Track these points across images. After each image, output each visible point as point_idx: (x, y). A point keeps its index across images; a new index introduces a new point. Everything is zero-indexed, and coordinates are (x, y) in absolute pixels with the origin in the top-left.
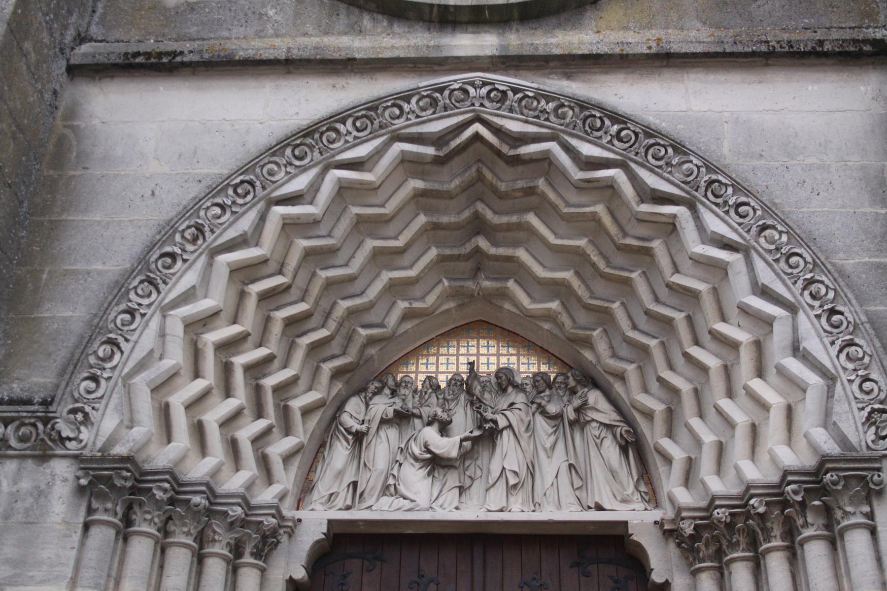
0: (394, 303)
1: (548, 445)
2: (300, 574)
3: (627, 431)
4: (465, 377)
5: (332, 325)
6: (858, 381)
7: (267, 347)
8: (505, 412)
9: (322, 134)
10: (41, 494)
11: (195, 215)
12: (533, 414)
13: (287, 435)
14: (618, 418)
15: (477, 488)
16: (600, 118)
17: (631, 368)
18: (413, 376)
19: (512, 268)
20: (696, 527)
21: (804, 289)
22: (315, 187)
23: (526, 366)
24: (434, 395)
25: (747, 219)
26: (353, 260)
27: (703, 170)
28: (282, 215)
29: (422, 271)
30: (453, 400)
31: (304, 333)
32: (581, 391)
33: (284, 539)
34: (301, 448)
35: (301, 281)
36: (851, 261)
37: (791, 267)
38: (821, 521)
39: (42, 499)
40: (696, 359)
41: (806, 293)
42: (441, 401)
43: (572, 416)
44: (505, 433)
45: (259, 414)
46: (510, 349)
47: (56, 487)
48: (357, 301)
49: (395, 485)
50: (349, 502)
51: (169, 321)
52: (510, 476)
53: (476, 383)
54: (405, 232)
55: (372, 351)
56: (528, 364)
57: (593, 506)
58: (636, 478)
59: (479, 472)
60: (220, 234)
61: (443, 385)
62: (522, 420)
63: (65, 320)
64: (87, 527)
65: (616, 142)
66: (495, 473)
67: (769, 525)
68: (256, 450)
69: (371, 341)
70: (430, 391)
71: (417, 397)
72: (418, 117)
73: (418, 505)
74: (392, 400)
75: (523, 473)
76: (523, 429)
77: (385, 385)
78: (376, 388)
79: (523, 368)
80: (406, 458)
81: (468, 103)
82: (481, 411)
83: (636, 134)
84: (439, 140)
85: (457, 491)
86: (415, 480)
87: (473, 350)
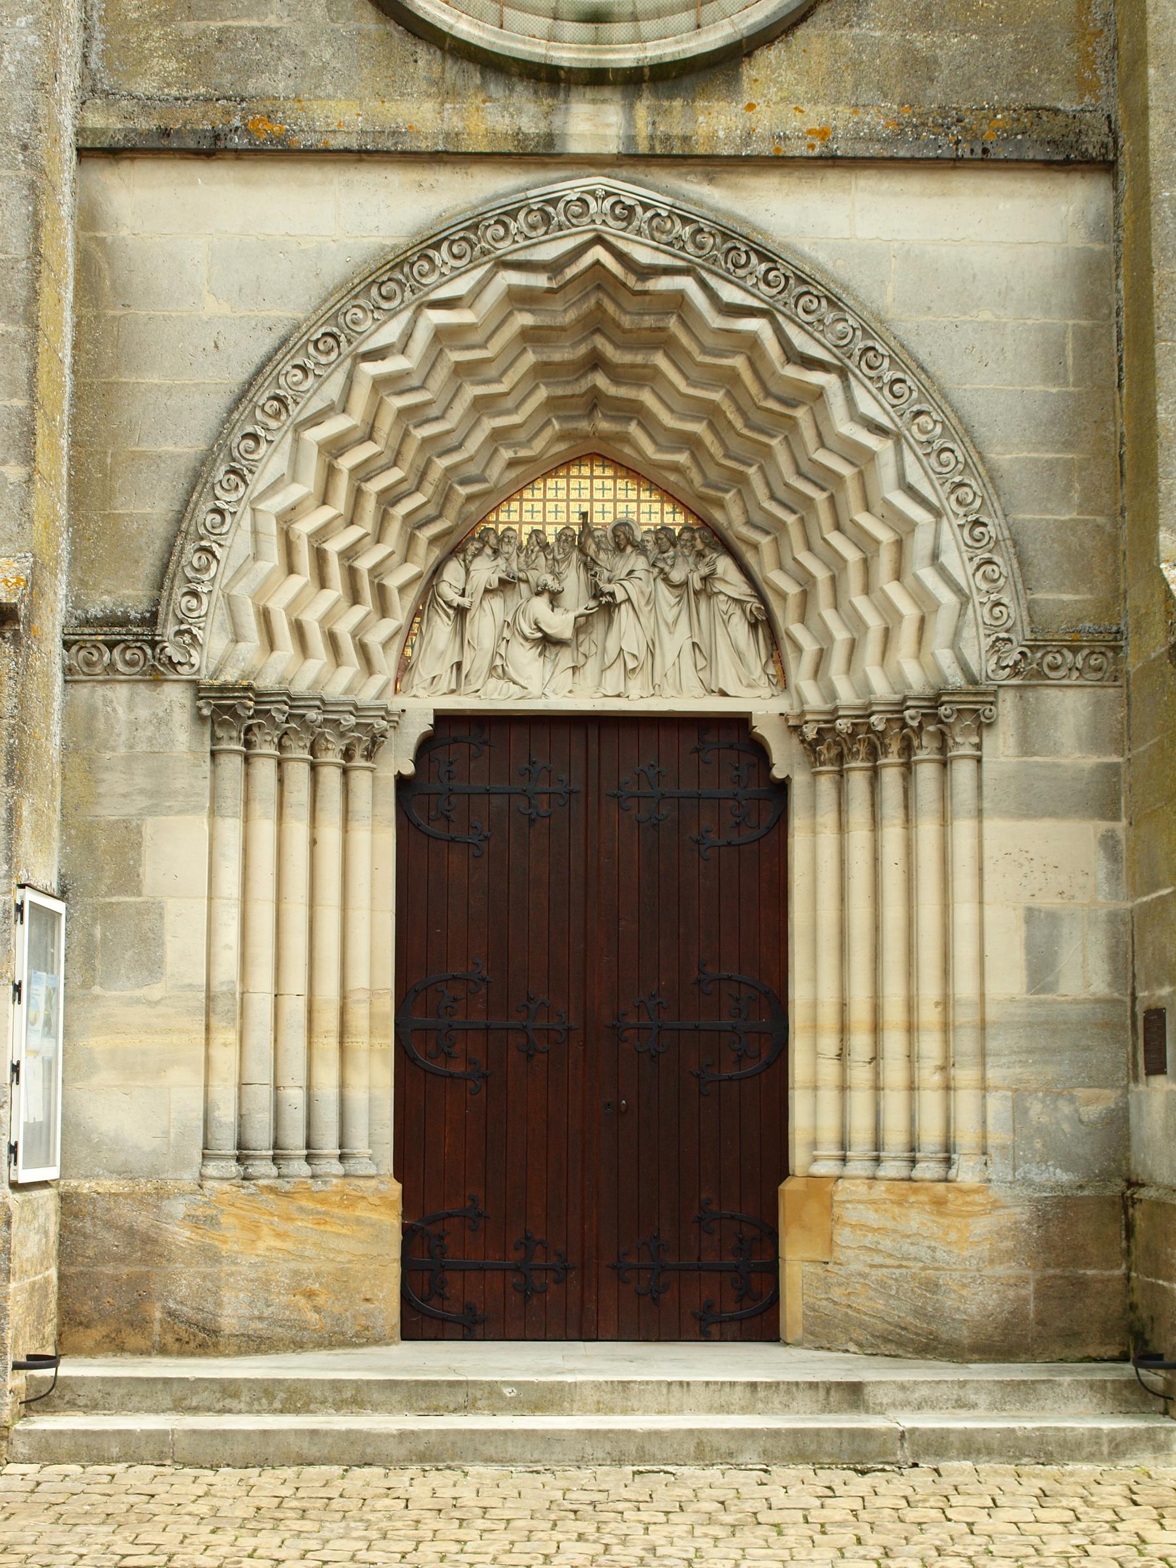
0: (496, 450)
1: (670, 620)
2: (409, 769)
3: (759, 609)
5: (429, 488)
6: (988, 606)
8: (623, 582)
9: (412, 265)
10: (161, 722)
11: (274, 384)
13: (384, 617)
15: (592, 667)
16: (746, 252)
17: (764, 541)
19: (634, 411)
21: (952, 492)
22: (408, 336)
23: (651, 513)
25: (902, 400)
26: (450, 411)
27: (859, 333)
36: (1008, 457)
37: (941, 464)
38: (936, 744)
39: (163, 727)
41: (953, 497)
42: (550, 562)
43: (698, 585)
44: (623, 606)
45: (355, 598)
47: (175, 715)
48: (455, 458)
50: (453, 686)
51: (260, 516)
52: (628, 658)
53: (590, 541)
54: (510, 373)
55: (472, 507)
59: (593, 649)
60: (305, 406)
61: (551, 540)
62: (642, 592)
63: (145, 517)
64: (213, 754)
65: (762, 286)
66: (612, 652)
67: (887, 741)
68: (354, 637)
69: (470, 498)
70: (537, 548)
71: (522, 555)
72: (527, 238)
74: (495, 563)
75: (643, 654)
76: (643, 602)
77: (485, 543)
79: (644, 519)
81: (586, 220)
83: (787, 278)
84: (553, 267)
85: (571, 671)
86: (524, 658)
87: (586, 494)
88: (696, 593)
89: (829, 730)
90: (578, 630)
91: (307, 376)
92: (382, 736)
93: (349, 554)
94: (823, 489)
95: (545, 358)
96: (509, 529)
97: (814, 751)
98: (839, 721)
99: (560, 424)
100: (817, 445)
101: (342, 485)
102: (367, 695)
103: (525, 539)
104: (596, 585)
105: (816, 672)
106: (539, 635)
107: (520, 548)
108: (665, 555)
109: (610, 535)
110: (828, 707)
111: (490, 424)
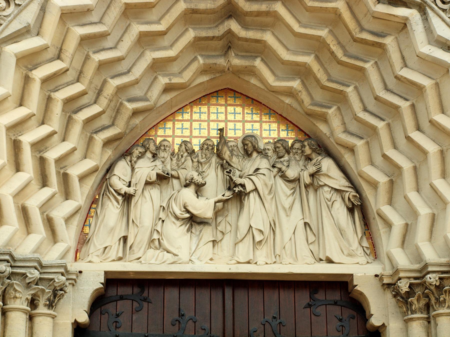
0: (156, 78)
1: (287, 206)
2: (83, 318)
3: (355, 196)
4: (215, 141)
7: (50, 125)
8: (251, 177)
12: (275, 177)
13: (67, 199)
14: (347, 184)
15: (228, 241)
17: (359, 144)
18: (170, 139)
19: (260, 50)
20: (411, 286)
23: (269, 131)
24: (189, 158)
26: (121, 43)
28: (60, 7)
29: (181, 51)
30: (206, 163)
31: (80, 109)
32: (316, 158)
33: (69, 289)
34: (80, 209)
35: (77, 65)
40: (417, 143)
42: (196, 164)
43: (308, 180)
44: (251, 195)
45: (44, 182)
46: (254, 116)
49: (159, 239)
50: (120, 255)
52: (256, 233)
53: (225, 149)
54: (167, 17)
55: (137, 121)
56: (270, 130)
57: (324, 259)
58: (360, 235)
59: (229, 228)
61: (197, 149)
62: (266, 185)
68: (42, 213)
69: (136, 113)
70: (186, 154)
71: (175, 159)
73: (180, 259)
74: (154, 164)
75: (267, 230)
76: (267, 192)
78: (140, 152)
79: (265, 134)
80: (168, 215)
82: (231, 175)
85: (211, 244)
86: (176, 233)
88: (306, 186)
89: (418, 285)
90: (217, 213)
91: (9, 5)
92: (61, 290)
93: (40, 146)
94: (406, 100)
95: (193, 6)
96: (165, 140)
97: (406, 302)
98: (428, 276)
99: (204, 59)
100: (402, 65)
101: (35, 92)
102: (52, 256)
103: (176, 148)
104: (231, 179)
105: (403, 242)
106: (188, 215)
107: (173, 154)
108: (282, 159)
109: (240, 145)
110: (417, 266)
111: (151, 55)
